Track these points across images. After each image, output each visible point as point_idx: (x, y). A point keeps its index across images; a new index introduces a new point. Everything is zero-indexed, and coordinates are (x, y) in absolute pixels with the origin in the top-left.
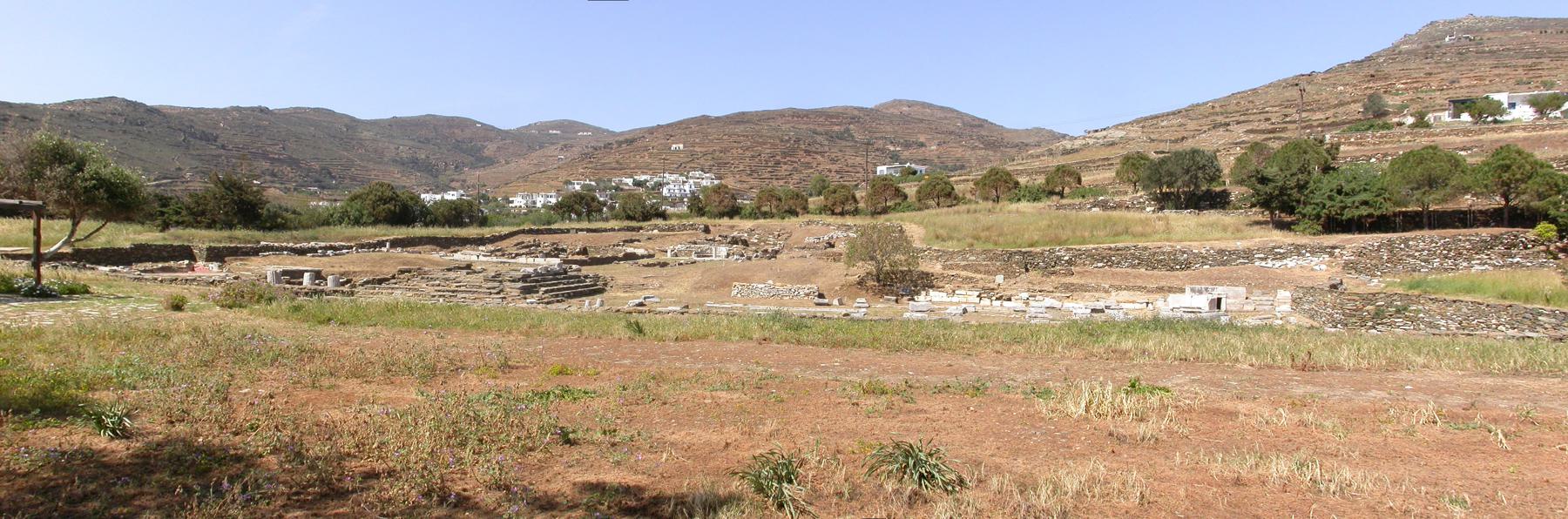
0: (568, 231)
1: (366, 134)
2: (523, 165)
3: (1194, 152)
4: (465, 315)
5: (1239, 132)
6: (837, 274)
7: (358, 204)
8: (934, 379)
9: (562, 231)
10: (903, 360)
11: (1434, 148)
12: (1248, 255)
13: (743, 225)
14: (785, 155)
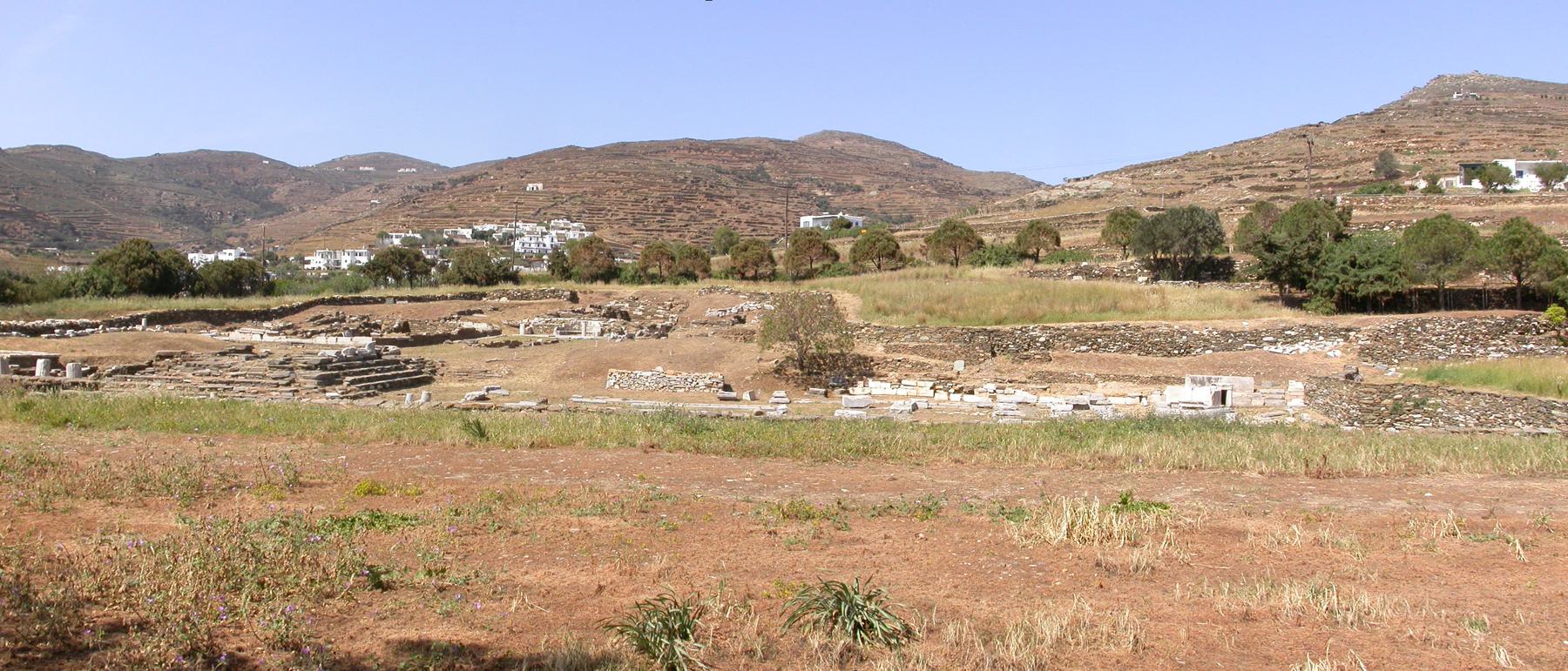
0: (383, 300)
1: (120, 178)
2: (325, 213)
3: (1193, 210)
4: (242, 414)
5: (1243, 189)
6: (750, 357)
7: (106, 269)
8: (874, 499)
9: (375, 301)
10: (834, 472)
11: (1448, 217)
12: (1256, 337)
13: (622, 293)
14: (679, 199)
